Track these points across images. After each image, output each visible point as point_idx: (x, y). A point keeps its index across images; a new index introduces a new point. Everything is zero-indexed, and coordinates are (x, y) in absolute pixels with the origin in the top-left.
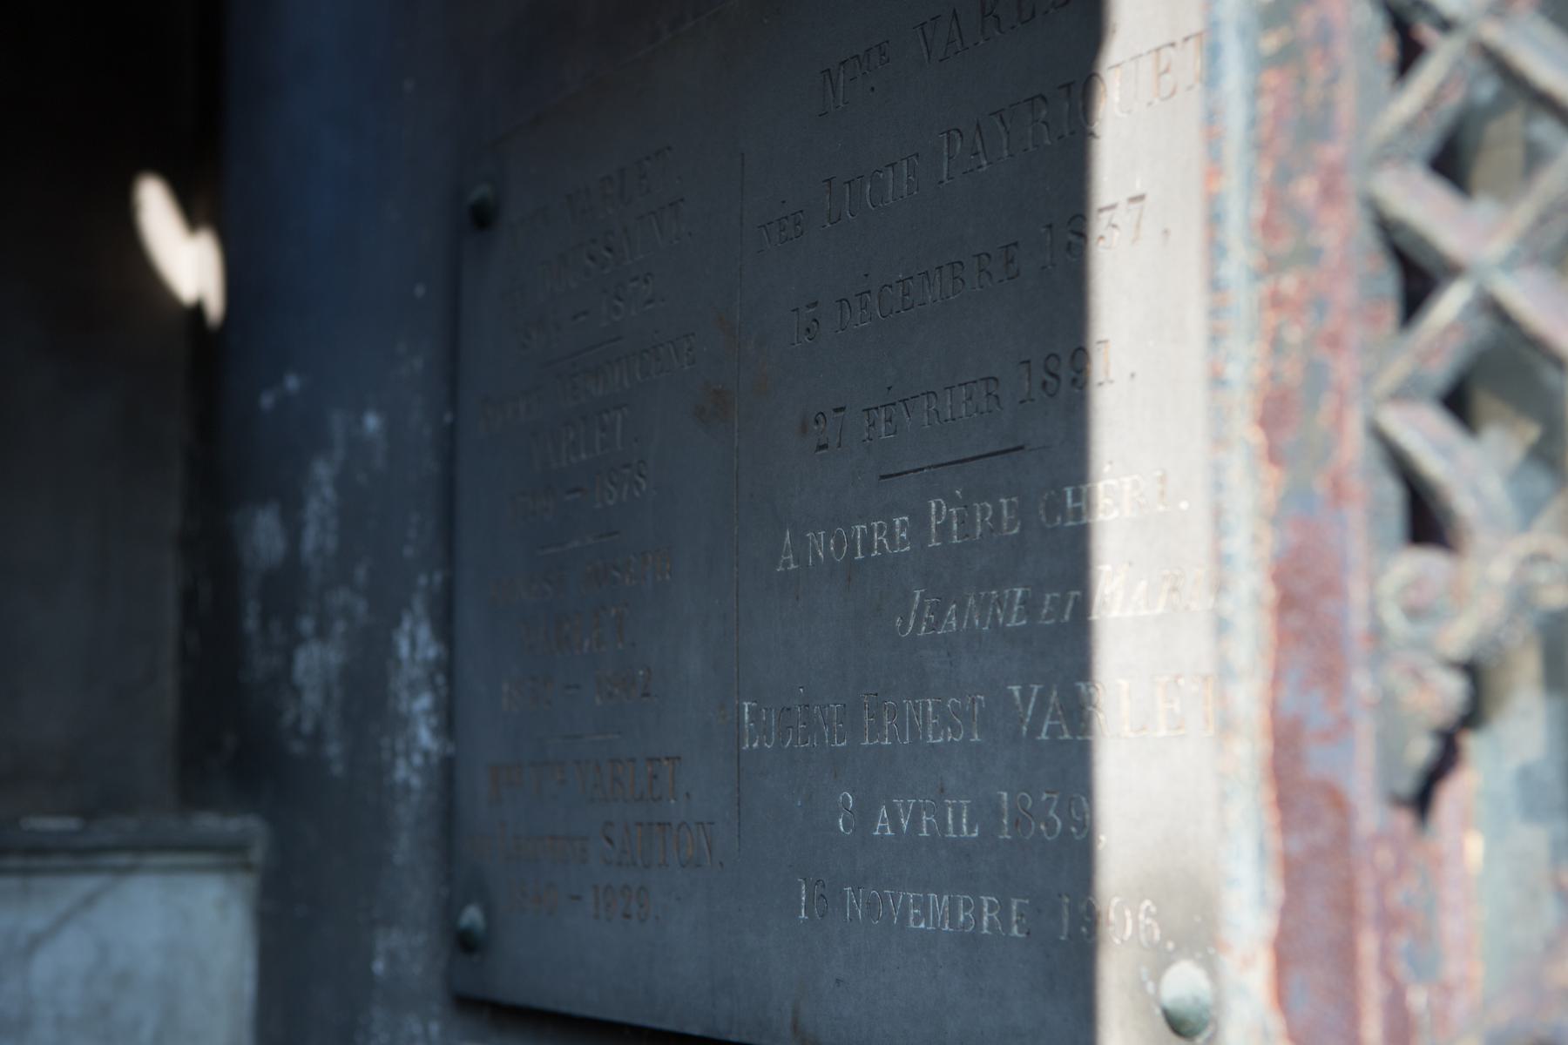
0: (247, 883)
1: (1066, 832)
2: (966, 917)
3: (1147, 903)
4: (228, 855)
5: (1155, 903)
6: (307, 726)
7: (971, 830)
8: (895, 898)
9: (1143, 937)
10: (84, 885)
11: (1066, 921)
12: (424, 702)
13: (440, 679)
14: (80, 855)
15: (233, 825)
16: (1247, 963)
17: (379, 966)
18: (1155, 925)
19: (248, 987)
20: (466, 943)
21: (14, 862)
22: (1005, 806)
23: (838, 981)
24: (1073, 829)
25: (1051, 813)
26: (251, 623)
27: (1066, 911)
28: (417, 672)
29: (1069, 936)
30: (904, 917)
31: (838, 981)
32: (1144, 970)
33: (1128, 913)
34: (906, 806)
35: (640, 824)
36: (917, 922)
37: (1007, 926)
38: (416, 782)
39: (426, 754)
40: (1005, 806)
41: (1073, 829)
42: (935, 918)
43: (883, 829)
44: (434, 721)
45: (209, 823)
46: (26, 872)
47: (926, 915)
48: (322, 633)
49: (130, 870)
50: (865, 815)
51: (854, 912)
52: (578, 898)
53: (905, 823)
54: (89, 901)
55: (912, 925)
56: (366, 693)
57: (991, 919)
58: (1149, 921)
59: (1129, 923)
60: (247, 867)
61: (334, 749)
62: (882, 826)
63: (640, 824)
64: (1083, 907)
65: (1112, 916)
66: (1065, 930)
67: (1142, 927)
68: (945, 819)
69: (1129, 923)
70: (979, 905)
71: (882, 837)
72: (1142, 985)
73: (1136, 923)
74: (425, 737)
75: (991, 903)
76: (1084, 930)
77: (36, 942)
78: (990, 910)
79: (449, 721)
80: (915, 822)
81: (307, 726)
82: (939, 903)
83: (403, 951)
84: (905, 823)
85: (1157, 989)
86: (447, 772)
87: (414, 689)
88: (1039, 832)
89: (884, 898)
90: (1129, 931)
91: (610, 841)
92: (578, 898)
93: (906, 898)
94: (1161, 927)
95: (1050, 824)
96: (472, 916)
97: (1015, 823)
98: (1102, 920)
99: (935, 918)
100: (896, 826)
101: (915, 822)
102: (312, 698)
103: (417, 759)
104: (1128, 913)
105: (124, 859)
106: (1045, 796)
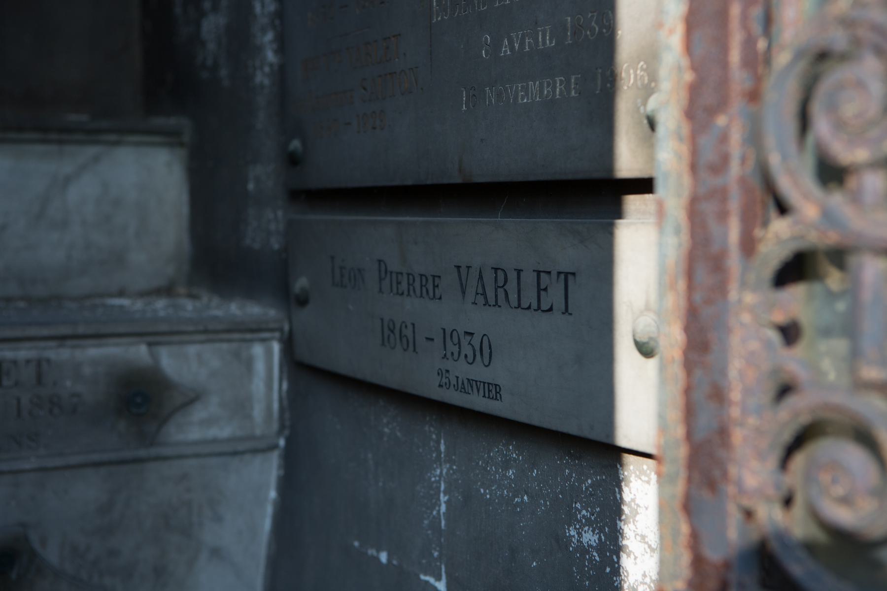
0: (182, 153)
1: (600, 32)
2: (548, 91)
3: (642, 63)
4: (171, 138)
5: (646, 63)
6: (209, 62)
7: (551, 43)
8: (511, 88)
9: (639, 83)
10: (91, 151)
11: (599, 82)
12: (269, 36)
13: (277, 22)
14: (90, 134)
15: (173, 121)
16: (671, 32)
17: (251, 186)
18: (645, 74)
19: (185, 210)
20: (293, 160)
21: (54, 136)
22: (569, 25)
23: (482, 140)
24: (604, 31)
25: (593, 24)
26: (178, 10)
27: (599, 76)
28: (265, 21)
29: (601, 90)
30: (516, 98)
31: (482, 140)
32: (639, 101)
33: (632, 71)
34: (517, 36)
35: (380, 76)
36: (523, 99)
37: (569, 92)
38: (266, 82)
39: (271, 65)
40: (569, 25)
41: (604, 31)
42: (532, 94)
43: (506, 51)
44: (275, 46)
45: (158, 121)
46: (60, 142)
47: (527, 95)
48: (215, 8)
49: (117, 143)
50: (496, 46)
51: (490, 101)
52: (349, 124)
53: (517, 46)
54: (96, 159)
55: (520, 101)
56: (239, 38)
57: (561, 89)
58: (642, 73)
59: (632, 76)
60: (181, 145)
61: (224, 73)
62: (505, 50)
63: (380, 76)
64: (608, 73)
65: (624, 75)
66: (599, 88)
67: (638, 77)
68: (538, 39)
69: (632, 76)
70: (555, 82)
71: (505, 56)
72: (638, 108)
73: (636, 75)
74: (270, 56)
75: (561, 80)
76: (609, 85)
77: (68, 180)
78: (560, 85)
79: (282, 44)
80: (522, 44)
81: (209, 62)
82: (534, 86)
83: (263, 175)
84: (517, 46)
85: (645, 109)
86: (281, 74)
87: (264, 31)
88: (586, 36)
89: (506, 90)
90: (632, 81)
91: (365, 89)
92: (349, 124)
93: (517, 87)
94: (648, 75)
95: (592, 30)
96: (296, 144)
97: (574, 33)
98: (618, 78)
99: (532, 94)
100: (512, 48)
101: (522, 44)
102: (211, 46)
103: (267, 69)
104: (632, 71)
105: (113, 137)
106: (590, 15)
